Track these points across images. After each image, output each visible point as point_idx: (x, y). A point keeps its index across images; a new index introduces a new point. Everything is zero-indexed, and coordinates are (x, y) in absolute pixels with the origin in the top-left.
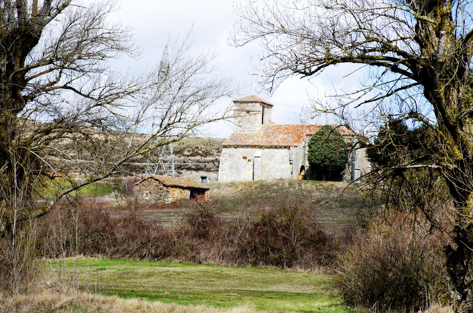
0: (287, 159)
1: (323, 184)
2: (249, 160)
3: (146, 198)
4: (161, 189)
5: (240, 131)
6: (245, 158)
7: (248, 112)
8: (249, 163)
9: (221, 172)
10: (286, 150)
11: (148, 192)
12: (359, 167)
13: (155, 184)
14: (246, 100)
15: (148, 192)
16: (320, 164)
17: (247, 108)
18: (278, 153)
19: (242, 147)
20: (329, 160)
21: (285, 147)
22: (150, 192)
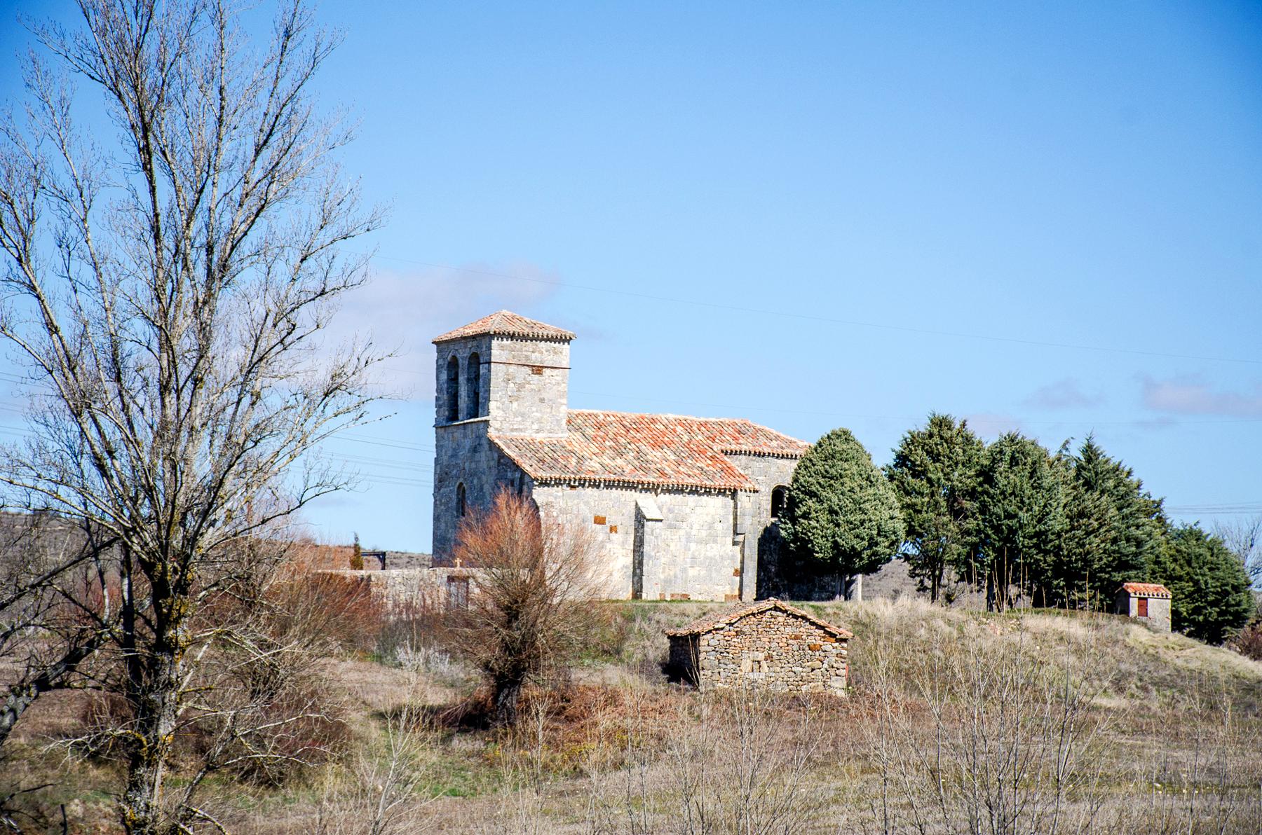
2: (613, 529)
5: (512, 430)
6: (600, 521)
7: (538, 370)
11: (761, 656)
13: (788, 629)
15: (761, 656)
17: (536, 359)
18: (698, 510)
22: (769, 658)
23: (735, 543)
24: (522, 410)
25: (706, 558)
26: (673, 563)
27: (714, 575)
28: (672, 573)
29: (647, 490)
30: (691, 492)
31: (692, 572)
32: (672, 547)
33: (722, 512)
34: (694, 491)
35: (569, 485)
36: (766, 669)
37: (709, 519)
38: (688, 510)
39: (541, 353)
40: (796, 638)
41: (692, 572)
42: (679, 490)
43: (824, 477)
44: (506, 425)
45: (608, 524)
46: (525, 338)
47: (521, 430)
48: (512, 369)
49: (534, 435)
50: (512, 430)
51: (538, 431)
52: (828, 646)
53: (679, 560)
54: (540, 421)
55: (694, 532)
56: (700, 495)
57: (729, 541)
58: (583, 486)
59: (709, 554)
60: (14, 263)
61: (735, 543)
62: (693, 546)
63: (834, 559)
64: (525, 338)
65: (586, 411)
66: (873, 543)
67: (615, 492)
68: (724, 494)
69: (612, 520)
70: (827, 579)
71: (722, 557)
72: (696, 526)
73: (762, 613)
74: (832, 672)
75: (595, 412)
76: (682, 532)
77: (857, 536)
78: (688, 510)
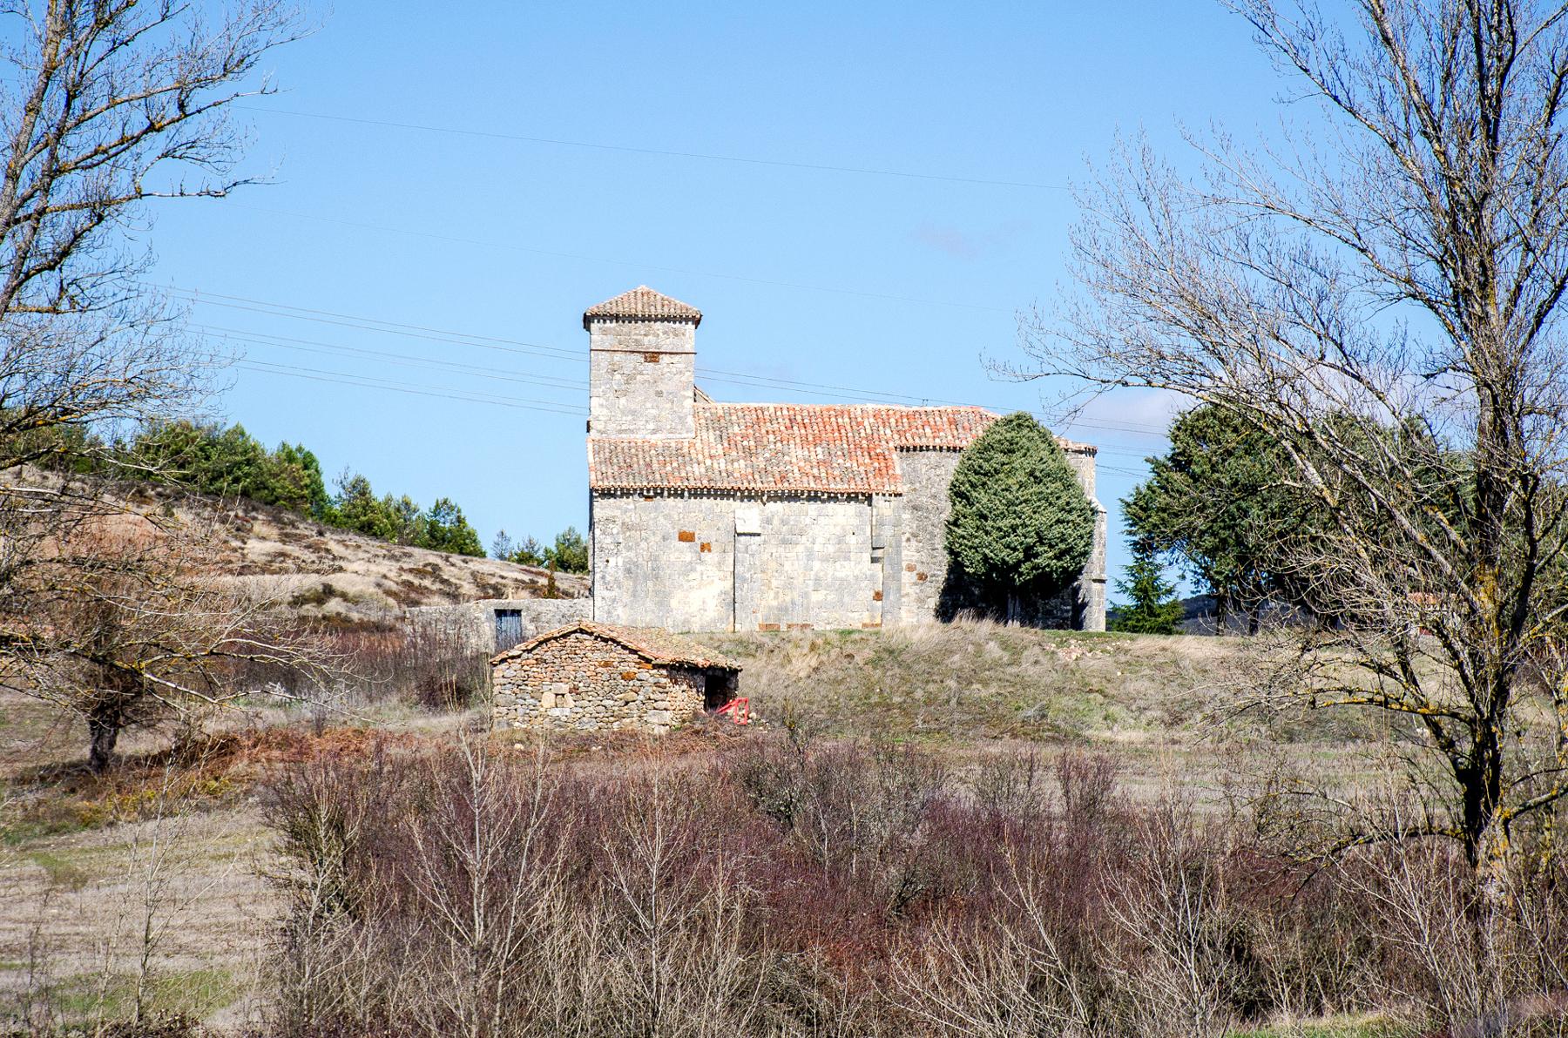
0: (858, 543)
1: (1127, 644)
2: (704, 547)
3: (556, 712)
4: (627, 677)
5: (620, 432)
6: (686, 537)
7: (653, 357)
8: (706, 556)
9: (607, 594)
10: (845, 513)
11: (564, 688)
12: (1102, 570)
13: (597, 655)
14: (620, 310)
15: (564, 688)
16: (1019, 563)
17: (649, 343)
18: (822, 520)
19: (677, 493)
20: (1051, 546)
21: (851, 497)
22: (574, 690)
23: (874, 560)
24: (633, 407)
25: (835, 579)
26: (789, 585)
27: (846, 599)
28: (788, 599)
29: (750, 498)
30: (809, 499)
31: (816, 597)
32: (788, 567)
33: (856, 522)
34: (814, 497)
35: (641, 494)
36: (572, 704)
37: (838, 531)
38: (808, 521)
39: (657, 336)
40: (607, 665)
41: (816, 597)
42: (793, 497)
43: (977, 473)
44: (611, 426)
45: (698, 542)
46: (632, 318)
47: (632, 431)
48: (618, 357)
49: (648, 437)
50: (620, 432)
51: (654, 432)
52: (644, 675)
53: (798, 582)
54: (656, 419)
55: (817, 547)
56: (823, 501)
57: (867, 557)
58: (661, 495)
59: (839, 575)
60: (1385, 150)
61: (874, 560)
62: (817, 565)
63: (988, 574)
64: (632, 318)
65: (753, 405)
66: (1029, 553)
67: (706, 502)
68: (856, 499)
69: (702, 535)
70: (1053, 602)
71: (856, 578)
72: (820, 540)
73: (564, 636)
74: (650, 705)
75: (765, 405)
76: (800, 548)
77: (1008, 546)
78: (808, 521)
